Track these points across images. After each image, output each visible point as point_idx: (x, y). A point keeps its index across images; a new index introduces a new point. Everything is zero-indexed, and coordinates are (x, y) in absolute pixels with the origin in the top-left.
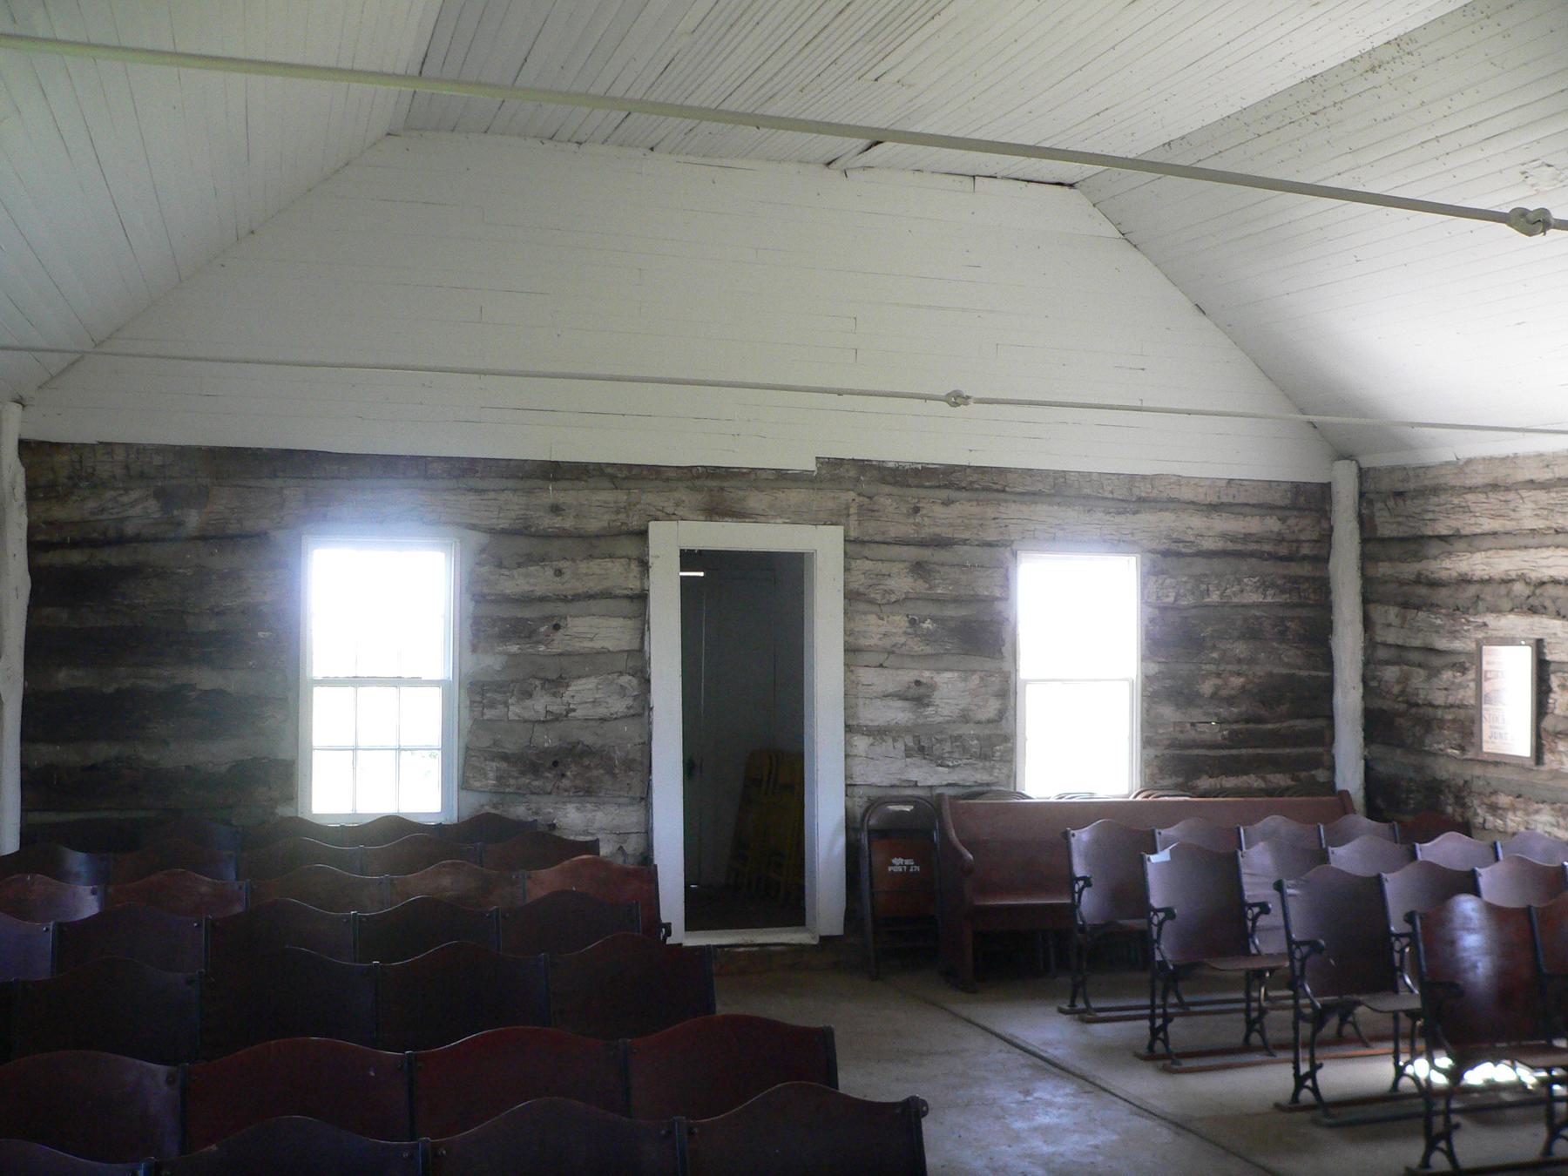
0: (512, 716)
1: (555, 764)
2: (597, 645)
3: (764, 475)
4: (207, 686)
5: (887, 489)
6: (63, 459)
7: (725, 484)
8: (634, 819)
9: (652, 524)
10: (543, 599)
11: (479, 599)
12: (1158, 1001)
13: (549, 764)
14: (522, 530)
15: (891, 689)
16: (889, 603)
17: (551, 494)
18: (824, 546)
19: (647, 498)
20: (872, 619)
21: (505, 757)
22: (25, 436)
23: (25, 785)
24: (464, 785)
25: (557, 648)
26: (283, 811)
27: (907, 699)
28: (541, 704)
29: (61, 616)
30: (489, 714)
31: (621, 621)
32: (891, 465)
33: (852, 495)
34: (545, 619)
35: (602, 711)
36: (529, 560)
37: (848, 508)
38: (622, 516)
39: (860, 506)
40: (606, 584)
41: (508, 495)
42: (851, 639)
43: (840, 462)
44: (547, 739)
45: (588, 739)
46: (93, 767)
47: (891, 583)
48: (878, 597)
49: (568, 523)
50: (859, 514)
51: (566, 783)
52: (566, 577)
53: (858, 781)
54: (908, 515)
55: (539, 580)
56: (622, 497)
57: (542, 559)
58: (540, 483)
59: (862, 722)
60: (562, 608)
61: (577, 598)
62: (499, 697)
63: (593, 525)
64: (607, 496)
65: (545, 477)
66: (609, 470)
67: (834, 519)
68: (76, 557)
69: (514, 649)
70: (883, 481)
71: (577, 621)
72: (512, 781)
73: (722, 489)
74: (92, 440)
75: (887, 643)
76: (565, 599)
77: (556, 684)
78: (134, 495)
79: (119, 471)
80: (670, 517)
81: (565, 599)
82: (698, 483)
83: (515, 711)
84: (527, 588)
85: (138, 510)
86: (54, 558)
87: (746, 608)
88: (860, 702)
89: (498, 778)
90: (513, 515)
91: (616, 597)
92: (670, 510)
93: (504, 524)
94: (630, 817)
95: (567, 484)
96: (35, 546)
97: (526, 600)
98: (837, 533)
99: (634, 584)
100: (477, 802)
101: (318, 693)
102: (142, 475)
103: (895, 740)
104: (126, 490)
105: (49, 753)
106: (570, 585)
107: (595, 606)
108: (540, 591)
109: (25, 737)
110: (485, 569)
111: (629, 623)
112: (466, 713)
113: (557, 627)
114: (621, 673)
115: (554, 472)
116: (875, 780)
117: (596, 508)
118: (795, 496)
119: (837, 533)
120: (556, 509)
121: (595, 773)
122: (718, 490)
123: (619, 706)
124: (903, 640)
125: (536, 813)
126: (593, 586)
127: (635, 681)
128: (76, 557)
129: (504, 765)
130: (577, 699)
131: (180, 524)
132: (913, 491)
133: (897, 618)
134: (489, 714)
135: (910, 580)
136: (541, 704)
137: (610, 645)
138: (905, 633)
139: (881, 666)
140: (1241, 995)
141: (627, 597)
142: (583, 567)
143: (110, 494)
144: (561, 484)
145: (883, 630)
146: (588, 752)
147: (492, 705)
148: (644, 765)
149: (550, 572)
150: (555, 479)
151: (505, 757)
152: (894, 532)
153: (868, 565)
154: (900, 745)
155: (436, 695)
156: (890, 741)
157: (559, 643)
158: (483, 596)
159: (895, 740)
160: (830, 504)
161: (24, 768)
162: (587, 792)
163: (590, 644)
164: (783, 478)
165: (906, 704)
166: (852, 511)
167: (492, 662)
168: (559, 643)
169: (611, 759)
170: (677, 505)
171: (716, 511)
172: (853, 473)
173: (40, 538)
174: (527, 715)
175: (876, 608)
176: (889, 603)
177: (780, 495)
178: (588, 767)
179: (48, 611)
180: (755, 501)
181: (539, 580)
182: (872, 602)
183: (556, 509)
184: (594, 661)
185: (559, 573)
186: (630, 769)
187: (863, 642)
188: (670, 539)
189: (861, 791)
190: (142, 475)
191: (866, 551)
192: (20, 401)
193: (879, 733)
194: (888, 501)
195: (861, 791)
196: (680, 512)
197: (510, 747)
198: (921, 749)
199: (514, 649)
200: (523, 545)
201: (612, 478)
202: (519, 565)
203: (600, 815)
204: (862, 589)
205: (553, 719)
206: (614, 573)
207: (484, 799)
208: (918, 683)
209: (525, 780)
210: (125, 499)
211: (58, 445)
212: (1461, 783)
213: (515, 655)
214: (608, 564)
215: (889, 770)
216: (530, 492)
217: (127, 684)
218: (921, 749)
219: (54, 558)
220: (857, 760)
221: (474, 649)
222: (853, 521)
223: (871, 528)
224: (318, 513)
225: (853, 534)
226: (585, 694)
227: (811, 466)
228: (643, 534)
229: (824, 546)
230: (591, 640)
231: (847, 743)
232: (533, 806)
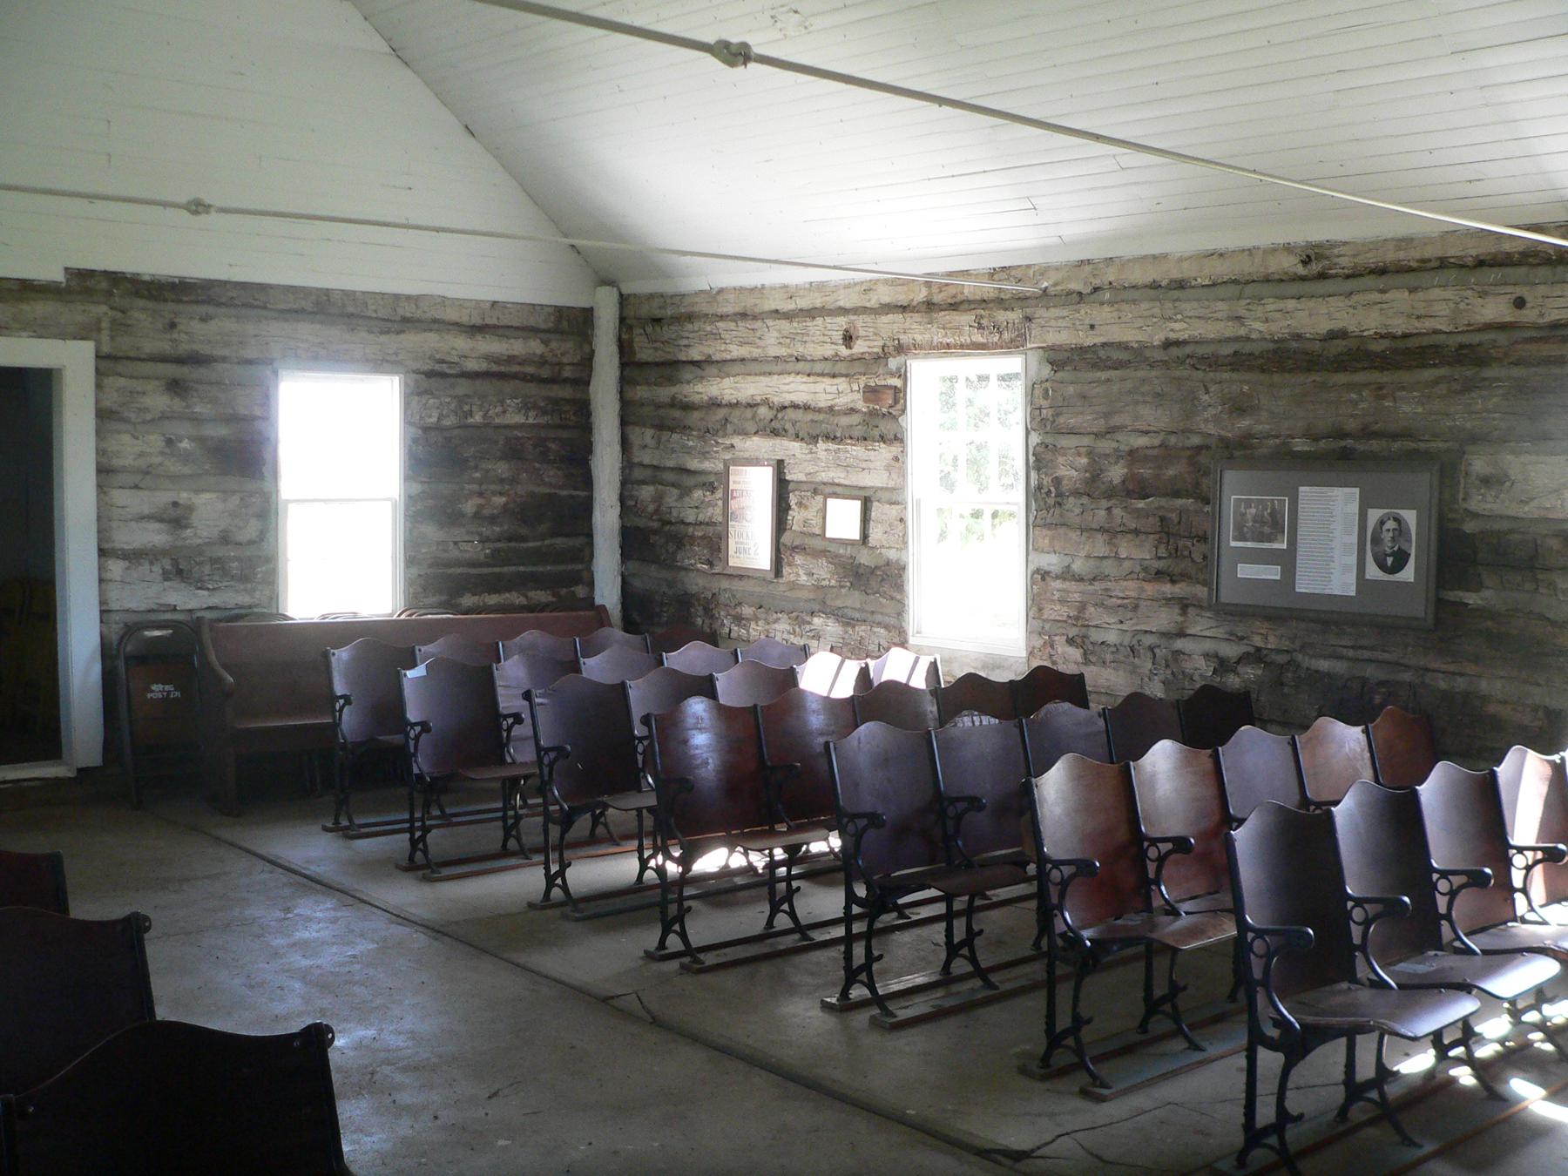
5: (141, 303)
12: (418, 815)
15: (146, 511)
18: (73, 362)
20: (126, 438)
27: (161, 520)
32: (147, 278)
37: (99, 321)
39: (113, 321)
47: (147, 401)
53: (114, 606)
70: (137, 294)
75: (141, 463)
88: (114, 524)
101: (290, 506)
103: (151, 563)
116: (132, 605)
118: (41, 308)
119: (87, 349)
133: (152, 438)
138: (162, 453)
139: (136, 487)
145: (137, 450)
152: (149, 347)
153: (122, 381)
154: (157, 569)
156: (147, 566)
159: (151, 563)
160: (80, 318)
176: (143, 422)
191: (120, 367)
193: (134, 556)
198: (180, 572)
215: (145, 593)
218: (180, 572)
223: (125, 344)
225: (106, 349)
227: (58, 276)
229: (73, 362)
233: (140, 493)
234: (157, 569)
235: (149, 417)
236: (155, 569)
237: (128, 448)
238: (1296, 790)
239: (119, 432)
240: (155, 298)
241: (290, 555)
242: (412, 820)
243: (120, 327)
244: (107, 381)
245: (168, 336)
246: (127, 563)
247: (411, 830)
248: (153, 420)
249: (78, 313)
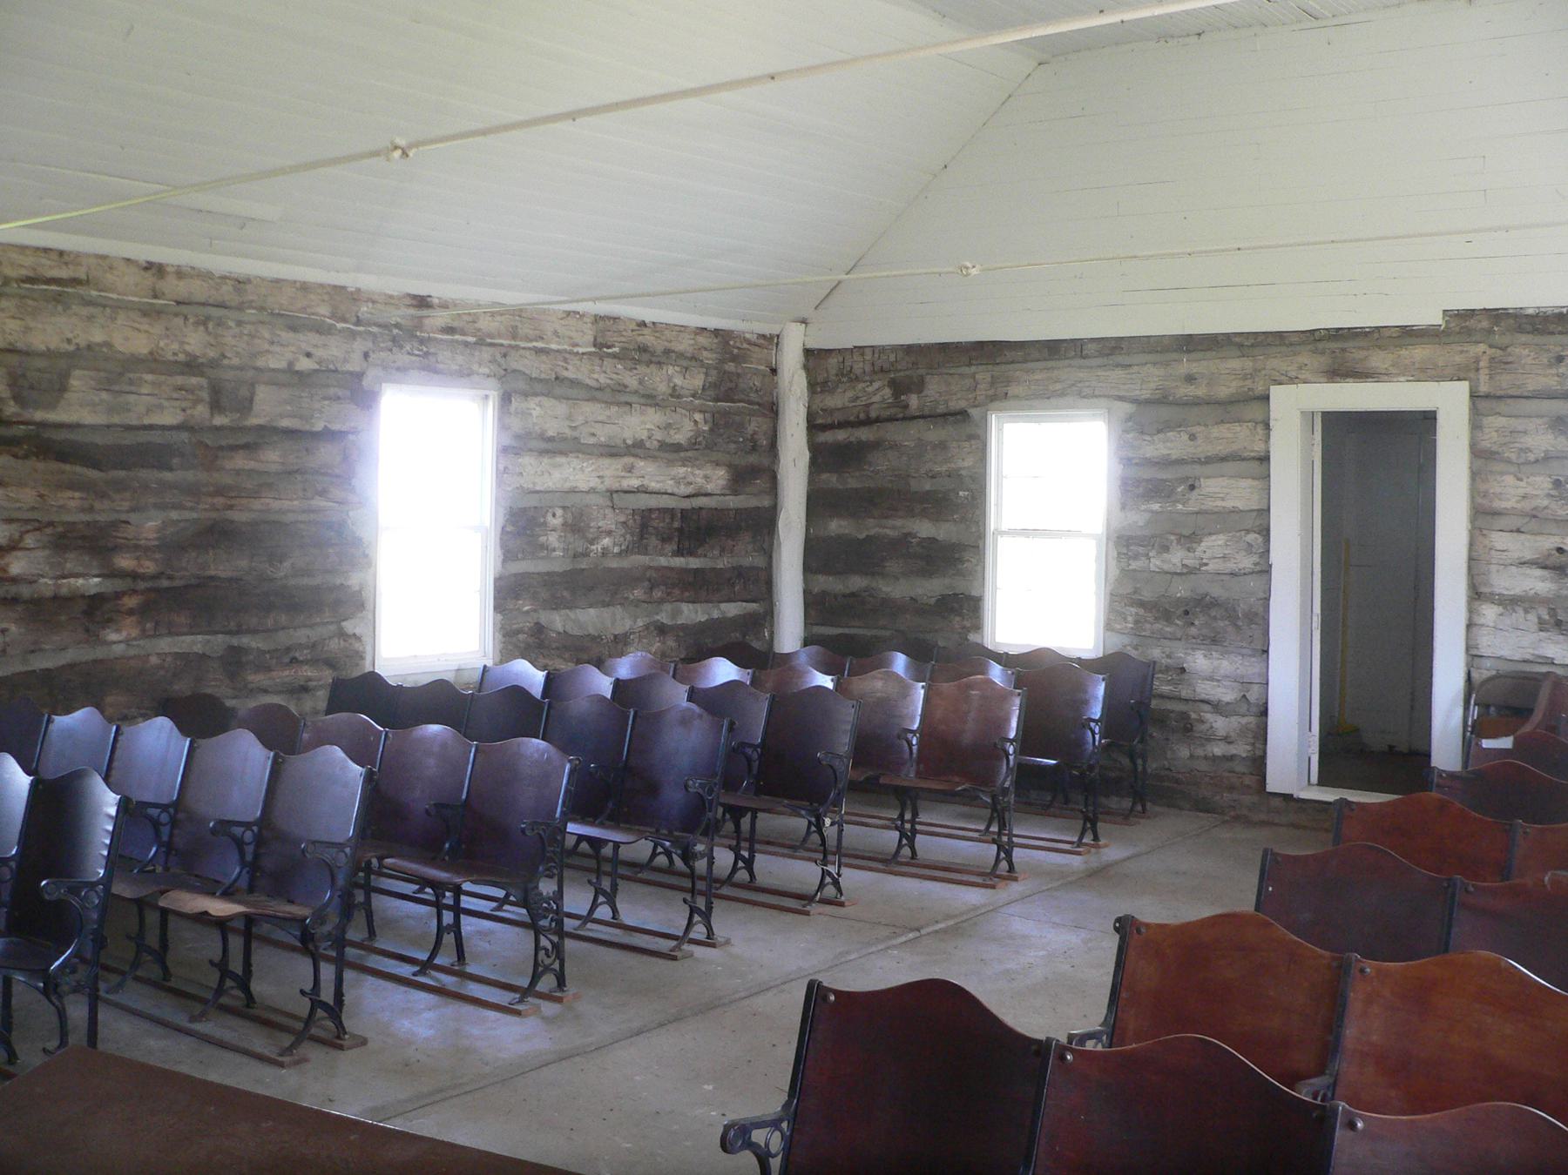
0: (1153, 568)
1: (1186, 613)
2: (1229, 504)
3: (1387, 333)
4: (924, 535)
5: (1524, 338)
6: (833, 361)
7: (1346, 345)
8: (1256, 670)
9: (1272, 388)
10: (1180, 462)
11: (1127, 462)
12: (908, 816)
13: (1180, 611)
14: (1162, 400)
15: (1528, 556)
16: (1528, 463)
17: (1186, 365)
18: (1449, 402)
19: (1273, 363)
20: (1510, 479)
21: (1142, 604)
22: (812, 345)
23: (807, 606)
24: (1109, 627)
25: (1193, 507)
26: (972, 637)
27: (1545, 568)
28: (1177, 557)
29: (830, 480)
30: (1134, 565)
31: (1250, 482)
32: (1530, 311)
33: (1482, 347)
34: (1183, 480)
35: (1230, 566)
36: (1165, 427)
37: (1477, 361)
38: (1249, 382)
39: (1492, 359)
40: (1235, 447)
41: (1150, 369)
42: (1480, 500)
43: (1471, 313)
44: (1181, 590)
45: (1216, 591)
46: (853, 595)
47: (1529, 441)
48: (1513, 457)
49: (1200, 391)
50: (1490, 368)
51: (1193, 631)
52: (1199, 441)
53: (1484, 651)
54: (1550, 366)
55: (1175, 445)
56: (1248, 364)
57: (1179, 425)
58: (1174, 356)
59: (1497, 591)
60: (1197, 470)
61: (1209, 460)
62: (1141, 550)
63: (1223, 392)
64: (1235, 364)
65: (1179, 349)
66: (1237, 339)
67: (1462, 375)
68: (841, 435)
69: (1156, 507)
70: (1520, 330)
71: (1210, 482)
72: (1148, 626)
73: (1343, 350)
74: (850, 346)
75: (1527, 506)
76: (1199, 462)
77: (1190, 539)
78: (876, 385)
79: (868, 368)
80: (1293, 380)
81: (1199, 462)
82: (1320, 345)
83: (1156, 563)
84: (1166, 452)
85: (876, 399)
86: (826, 437)
87: (1375, 464)
88: (1494, 568)
89: (1136, 622)
90: (1153, 386)
91: (1244, 459)
92: (1293, 374)
93: (1146, 394)
94: (1248, 668)
95: (1200, 355)
96: (813, 426)
97: (1166, 463)
98: (1463, 387)
99: (1259, 447)
100: (1117, 643)
101: (1003, 542)
102: (882, 370)
103: (1526, 611)
104: (871, 382)
105: (825, 582)
106: (1203, 449)
107: (1230, 467)
108: (1175, 454)
109: (809, 568)
110: (1131, 435)
111: (1256, 483)
112: (1113, 563)
113: (1192, 487)
114: (1248, 531)
115: (1190, 344)
116: (1506, 653)
117: (1226, 375)
118: (1420, 353)
119: (1463, 387)
120: (1190, 379)
121: (1221, 624)
122: (1341, 352)
123: (1247, 562)
124: (1546, 502)
125: (1169, 656)
126: (1221, 449)
127: (1260, 539)
128: (841, 435)
129: (1141, 611)
130: (1208, 555)
131: (906, 406)
132: (1552, 339)
133: (1538, 479)
134: (1134, 565)
135: (1551, 436)
136: (1177, 557)
137: (1240, 505)
138: (1549, 496)
139: (1518, 531)
140: (982, 827)
141: (1253, 458)
142: (1215, 431)
143: (861, 386)
144: (1194, 355)
145: (1521, 492)
146: (1215, 603)
147: (1136, 557)
148: (1258, 620)
149: (1185, 437)
150: (1188, 351)
151: (1142, 604)
152: (1533, 384)
153: (1500, 421)
154: (1532, 617)
155: (1093, 543)
156: (1521, 612)
157: (1194, 502)
158: (1129, 459)
159: (1526, 611)
160: (1458, 359)
161: (807, 593)
162: (1214, 641)
163: (1219, 503)
164: (1408, 334)
165: (1545, 573)
166: (1482, 364)
167: (1137, 518)
168: (1194, 502)
169: (1234, 610)
170: (1300, 368)
171: (1339, 372)
172: (1485, 324)
173: (820, 421)
174: (1166, 567)
175: (1513, 469)
176: (1528, 463)
177: (1403, 352)
178: (1215, 618)
179: (825, 476)
180: (1378, 360)
181: (1175, 445)
182: (1509, 461)
183: (1190, 379)
184: (1225, 520)
185: (1193, 437)
186: (1251, 622)
187: (1499, 505)
188: (1298, 405)
189: (1488, 663)
190: (882, 370)
191: (1502, 406)
192: (804, 322)
193: (1510, 603)
194: (1524, 351)
195: (1488, 663)
196: (1304, 375)
197: (1147, 595)
198: (1558, 624)
199: (1156, 507)
200: (1165, 413)
201: (1241, 346)
202: (1159, 431)
203: (1225, 663)
204: (1495, 448)
205: (1190, 571)
206: (1238, 436)
207: (1126, 640)
208: (1560, 550)
209: (1158, 626)
210: (870, 389)
211: (830, 351)
212: (813, 649)
213: (1157, 512)
214: (1237, 427)
215: (1516, 643)
216: (1167, 364)
217: (872, 532)
218: (1558, 624)
219: (826, 437)
220: (1484, 631)
221: (1123, 507)
222: (1483, 377)
223: (1505, 381)
224: (999, 396)
225: (1484, 388)
226: (1213, 547)
227: (1436, 319)
228: (1267, 398)
229: (1449, 402)
230: (1223, 499)
231: (1471, 611)
232: (1167, 650)
233: (1523, 536)
234: (1532, 617)
235: (1532, 457)
236: (1529, 617)
237: (1510, 491)
238: (517, 929)
239: (1502, 474)
240: (1535, 331)
241: (1093, 587)
242: (901, 816)
243: (1500, 364)
244: (1487, 421)
245: (1554, 371)
246: (1501, 609)
247: (900, 829)
248: (1537, 461)
249: (1456, 355)
